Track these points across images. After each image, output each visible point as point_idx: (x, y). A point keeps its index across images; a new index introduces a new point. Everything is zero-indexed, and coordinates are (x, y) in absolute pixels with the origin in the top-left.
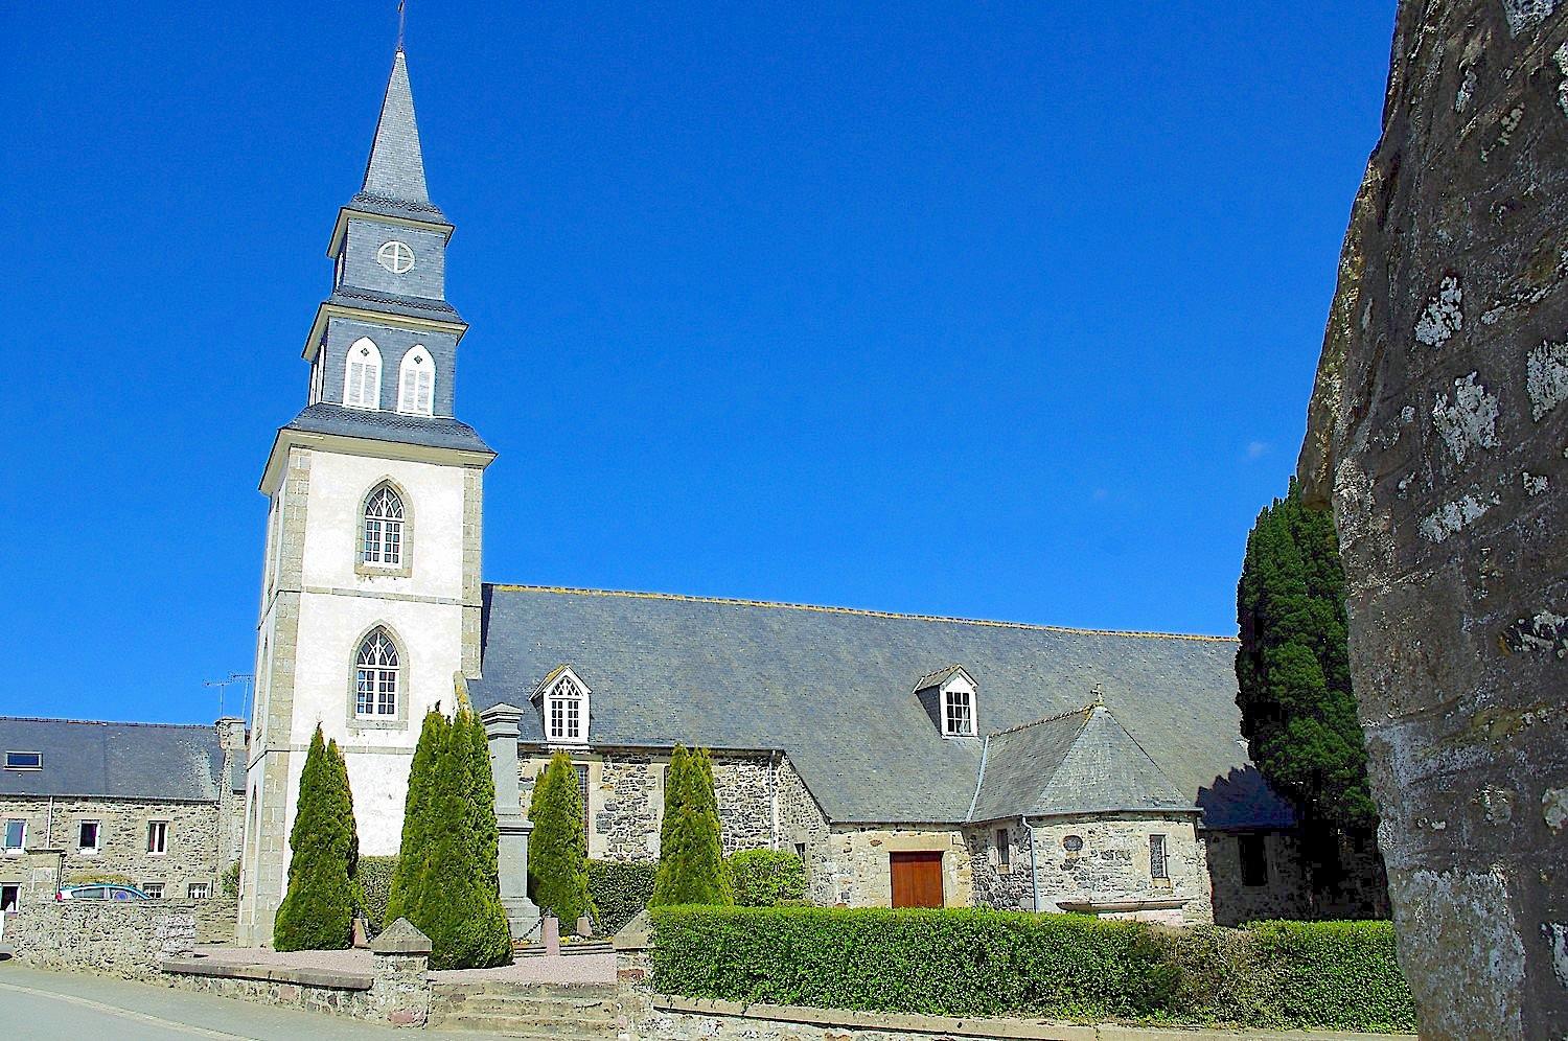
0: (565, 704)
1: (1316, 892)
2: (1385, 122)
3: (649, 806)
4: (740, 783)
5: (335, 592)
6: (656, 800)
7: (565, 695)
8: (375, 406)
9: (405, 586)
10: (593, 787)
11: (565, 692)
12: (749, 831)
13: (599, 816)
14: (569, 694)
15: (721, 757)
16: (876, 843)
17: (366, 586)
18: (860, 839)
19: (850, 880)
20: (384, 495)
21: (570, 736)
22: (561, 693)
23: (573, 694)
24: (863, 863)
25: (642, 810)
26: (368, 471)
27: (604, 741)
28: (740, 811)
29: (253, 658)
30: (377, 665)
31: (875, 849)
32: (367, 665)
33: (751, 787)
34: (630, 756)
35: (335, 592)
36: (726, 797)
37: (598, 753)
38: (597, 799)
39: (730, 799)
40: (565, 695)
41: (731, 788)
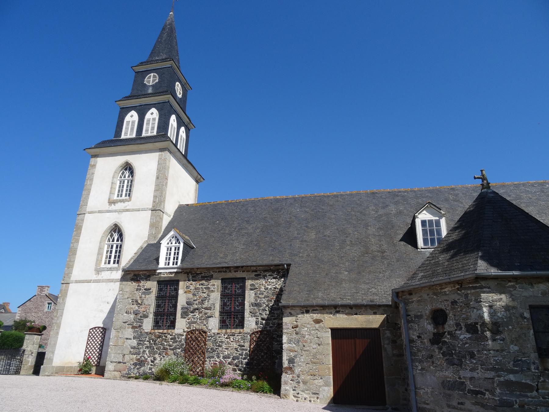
0: (173, 249)
1: (499, 400)
3: (211, 302)
5: (100, 212)
8: (134, 136)
10: (181, 292)
13: (182, 308)
14: (176, 243)
15: (256, 271)
16: (318, 321)
17: (113, 207)
18: (307, 318)
19: (296, 349)
20: (128, 168)
22: (172, 243)
23: (170, 243)
24: (307, 336)
25: (206, 304)
27: (188, 265)
28: (267, 304)
29: (141, 254)
30: (115, 242)
31: (317, 326)
32: (111, 243)
33: (275, 288)
34: (202, 273)
35: (100, 212)
37: (185, 273)
38: (182, 299)
41: (261, 289)
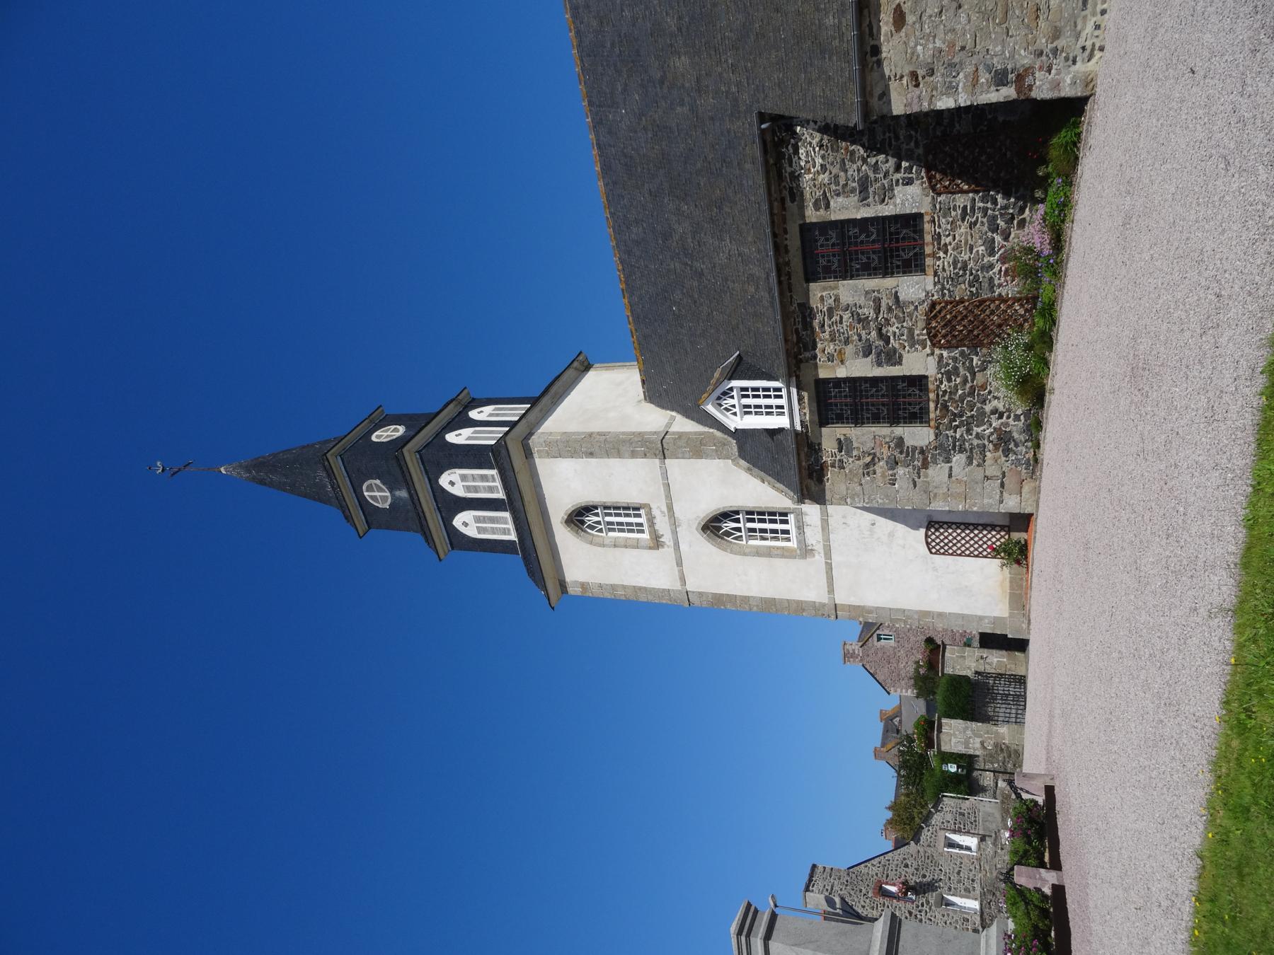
0: (745, 401)
2: (348, 518)
3: (862, 301)
4: (818, 167)
5: (679, 563)
6: (851, 291)
7: (735, 402)
9: (659, 508)
10: (841, 373)
11: (731, 402)
12: (890, 145)
14: (732, 397)
15: (783, 200)
20: (578, 518)
21: (781, 397)
22: (734, 406)
25: (868, 311)
26: (564, 537)
28: (860, 163)
31: (910, 19)
34: (797, 330)
35: (679, 563)
36: (839, 188)
39: (842, 182)
40: (735, 402)
